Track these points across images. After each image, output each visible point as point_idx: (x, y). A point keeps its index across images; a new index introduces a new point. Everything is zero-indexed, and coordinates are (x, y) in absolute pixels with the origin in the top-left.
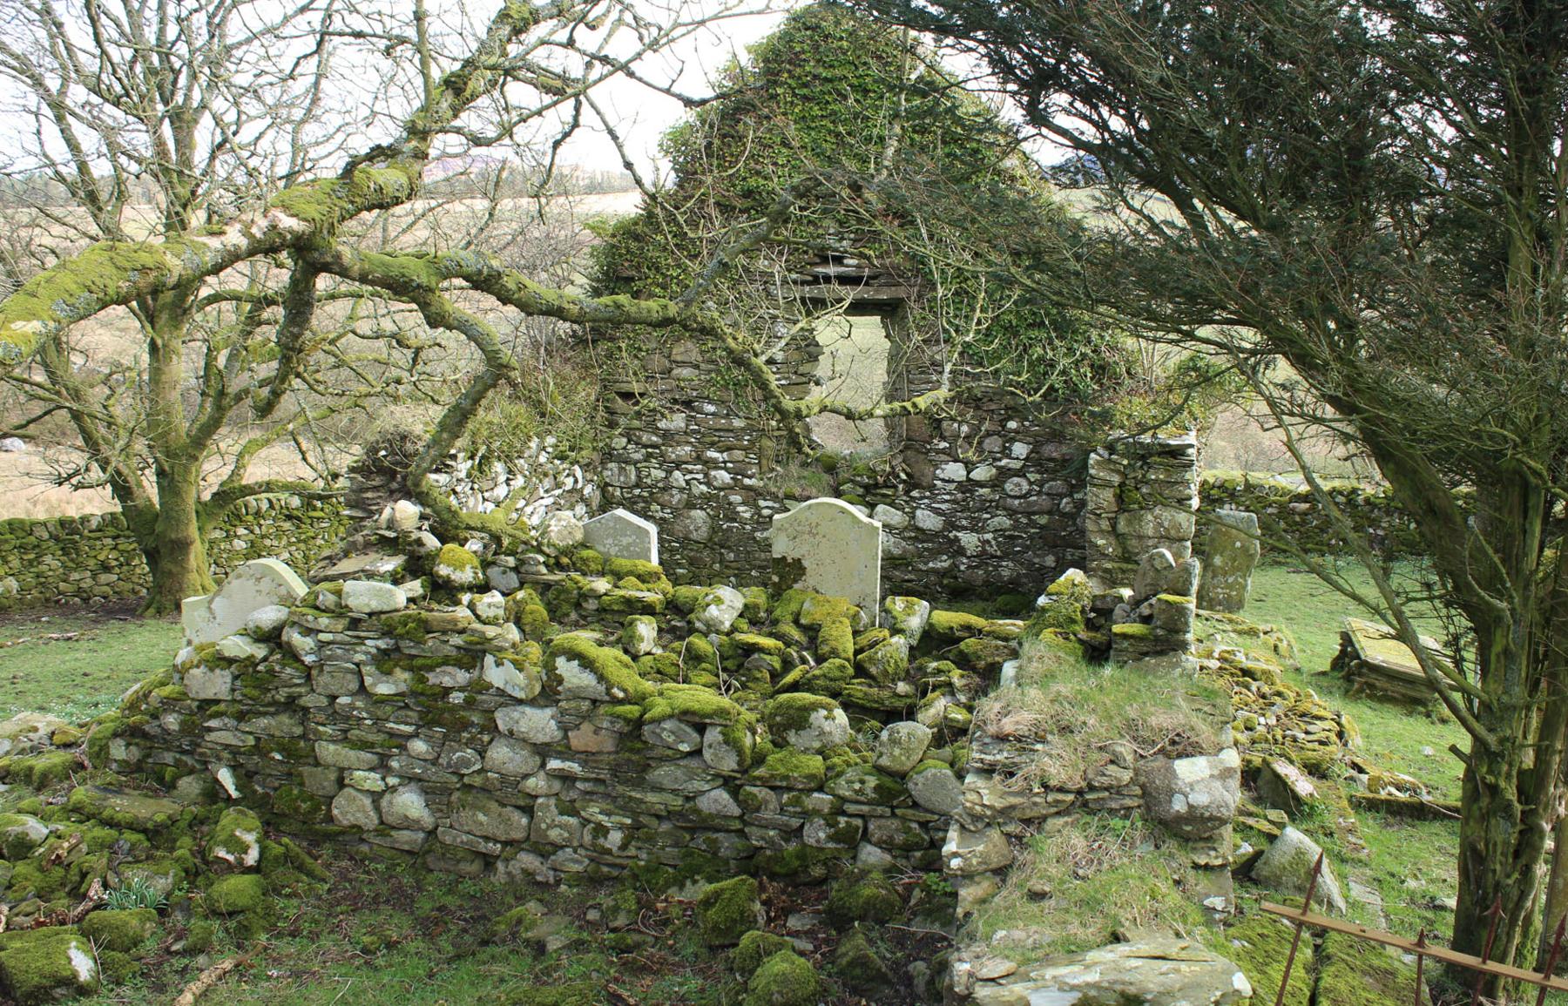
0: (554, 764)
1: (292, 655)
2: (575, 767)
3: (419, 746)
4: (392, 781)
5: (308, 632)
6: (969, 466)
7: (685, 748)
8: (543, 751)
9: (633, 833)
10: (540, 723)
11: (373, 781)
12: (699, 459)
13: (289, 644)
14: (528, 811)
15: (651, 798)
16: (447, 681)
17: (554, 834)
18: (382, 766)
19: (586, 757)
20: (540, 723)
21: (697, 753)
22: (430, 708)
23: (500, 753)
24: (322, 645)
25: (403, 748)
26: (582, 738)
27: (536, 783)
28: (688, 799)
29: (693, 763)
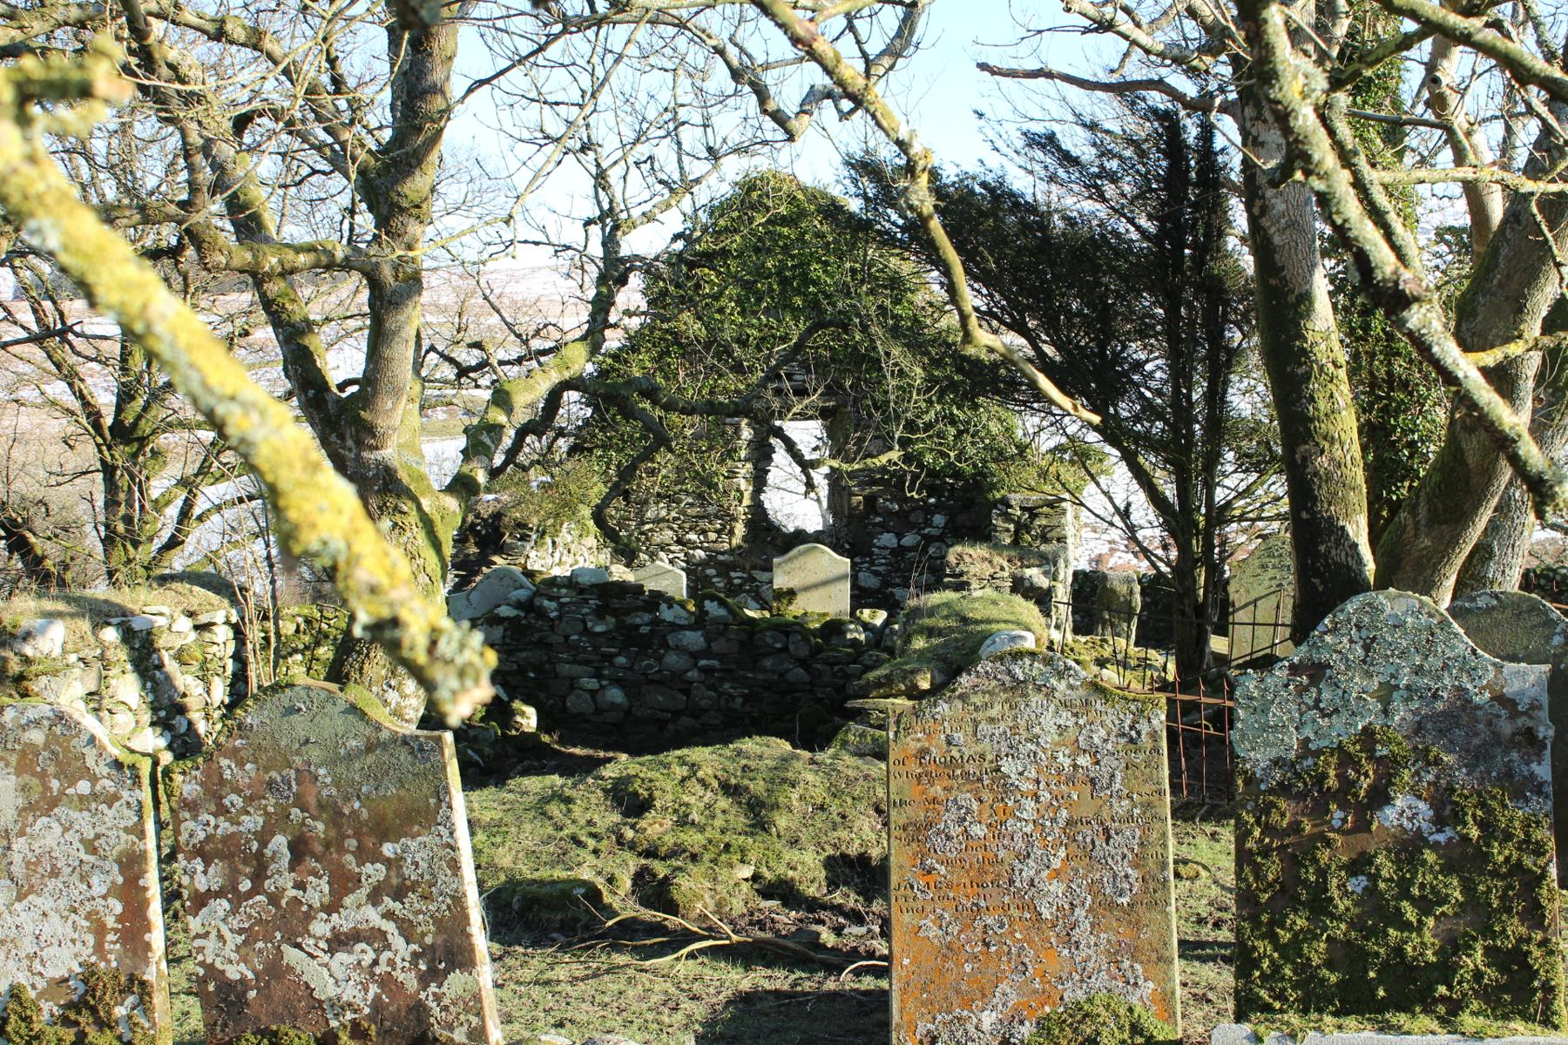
0: (703, 662)
1: (542, 613)
2: (716, 663)
3: (621, 660)
4: (604, 683)
5: (551, 599)
6: (900, 536)
7: (778, 645)
8: (695, 656)
9: (746, 698)
10: (694, 639)
11: (592, 684)
12: (679, 542)
13: (541, 606)
14: (687, 692)
15: (761, 676)
16: (638, 621)
17: (704, 703)
18: (598, 675)
19: (720, 657)
20: (694, 639)
21: (785, 649)
22: (628, 637)
23: (671, 659)
24: (562, 605)
25: (612, 664)
26: (719, 646)
27: (693, 674)
28: (781, 675)
29: (784, 655)
